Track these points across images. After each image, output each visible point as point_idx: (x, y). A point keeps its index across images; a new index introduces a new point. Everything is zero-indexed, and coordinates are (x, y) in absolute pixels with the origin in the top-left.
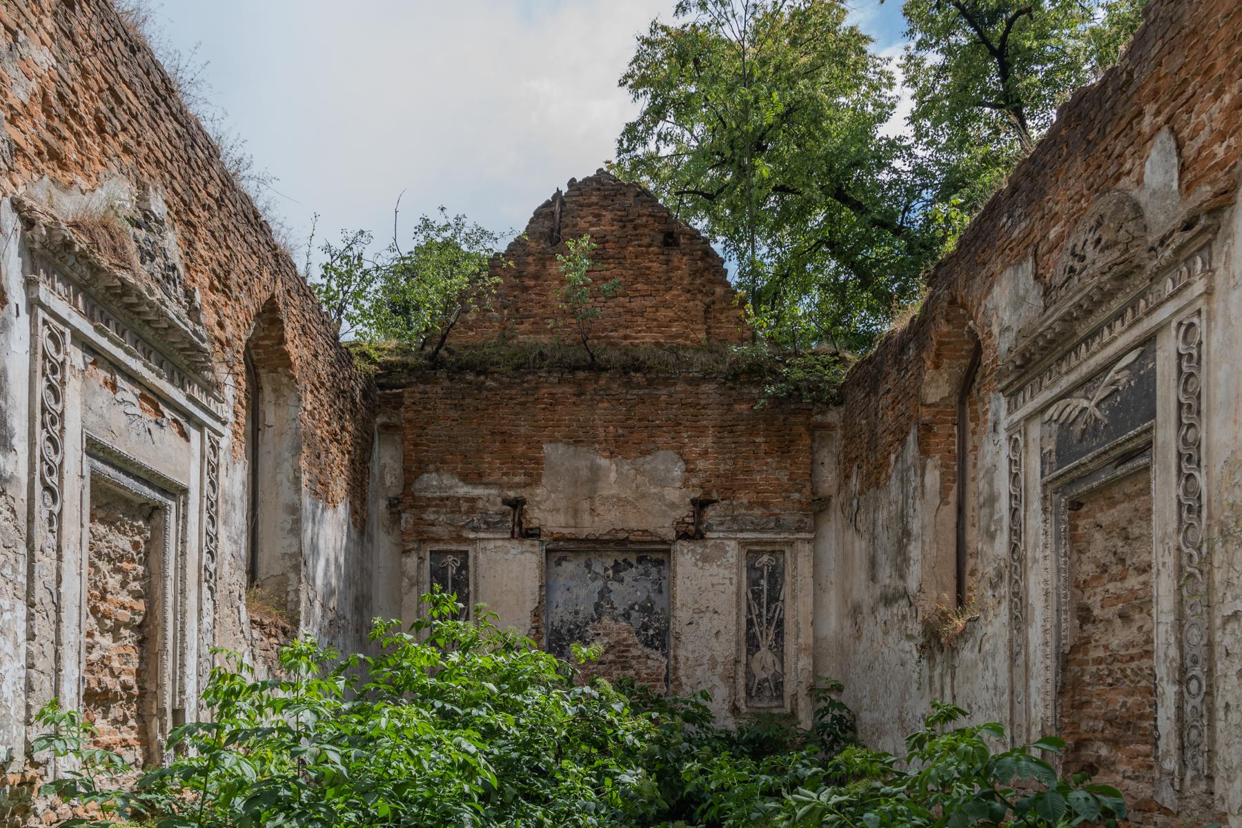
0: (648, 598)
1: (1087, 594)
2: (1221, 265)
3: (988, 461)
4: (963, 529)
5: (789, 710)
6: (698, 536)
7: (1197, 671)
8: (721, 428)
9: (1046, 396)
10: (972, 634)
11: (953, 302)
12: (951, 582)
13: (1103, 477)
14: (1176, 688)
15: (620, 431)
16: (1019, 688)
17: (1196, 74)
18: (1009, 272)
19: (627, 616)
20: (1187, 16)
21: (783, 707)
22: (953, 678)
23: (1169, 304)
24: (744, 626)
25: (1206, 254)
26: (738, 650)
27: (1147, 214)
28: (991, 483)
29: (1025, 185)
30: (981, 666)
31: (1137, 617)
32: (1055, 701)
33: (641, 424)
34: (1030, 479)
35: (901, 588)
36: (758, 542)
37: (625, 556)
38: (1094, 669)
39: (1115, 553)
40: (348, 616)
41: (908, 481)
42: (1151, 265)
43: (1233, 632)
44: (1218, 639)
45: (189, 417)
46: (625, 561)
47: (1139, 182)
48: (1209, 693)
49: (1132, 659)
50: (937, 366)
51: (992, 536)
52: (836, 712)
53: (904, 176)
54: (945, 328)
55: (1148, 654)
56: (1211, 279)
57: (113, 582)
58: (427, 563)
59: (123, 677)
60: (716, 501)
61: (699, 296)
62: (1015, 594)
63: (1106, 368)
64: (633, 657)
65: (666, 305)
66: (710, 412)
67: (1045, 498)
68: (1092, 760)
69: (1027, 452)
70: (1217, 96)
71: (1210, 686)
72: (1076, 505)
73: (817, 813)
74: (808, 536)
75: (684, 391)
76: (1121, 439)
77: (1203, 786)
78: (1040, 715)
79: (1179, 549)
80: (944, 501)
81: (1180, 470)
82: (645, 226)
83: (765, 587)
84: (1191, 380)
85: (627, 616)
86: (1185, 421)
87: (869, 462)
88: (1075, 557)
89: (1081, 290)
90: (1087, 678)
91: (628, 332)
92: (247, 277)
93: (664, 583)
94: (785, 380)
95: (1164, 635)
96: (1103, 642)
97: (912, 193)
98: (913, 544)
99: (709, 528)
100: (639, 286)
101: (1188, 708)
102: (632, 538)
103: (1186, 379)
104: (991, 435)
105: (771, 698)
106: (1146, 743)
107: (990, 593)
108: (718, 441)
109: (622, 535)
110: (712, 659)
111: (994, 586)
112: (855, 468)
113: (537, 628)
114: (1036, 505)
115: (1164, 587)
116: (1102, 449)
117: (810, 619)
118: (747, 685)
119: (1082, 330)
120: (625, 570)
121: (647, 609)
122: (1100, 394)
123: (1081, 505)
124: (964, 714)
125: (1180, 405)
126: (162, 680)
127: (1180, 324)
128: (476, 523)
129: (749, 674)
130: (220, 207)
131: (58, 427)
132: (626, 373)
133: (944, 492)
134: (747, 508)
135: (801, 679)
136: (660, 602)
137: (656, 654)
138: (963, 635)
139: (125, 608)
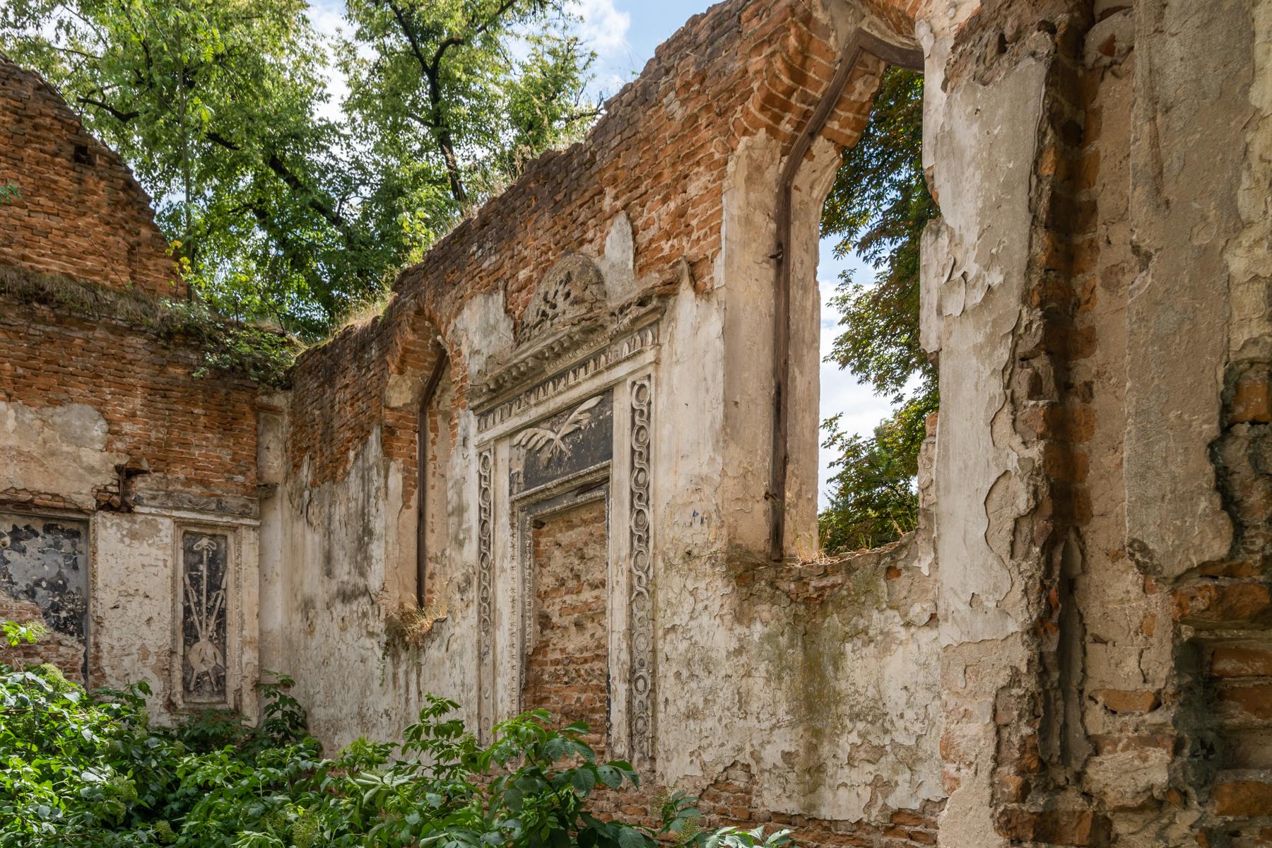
0: (60, 574)
1: (546, 604)
3: (457, 472)
4: (424, 533)
5: (232, 706)
6: (124, 509)
7: (643, 672)
8: (152, 390)
10: (439, 634)
11: (419, 312)
12: (411, 583)
13: (565, 503)
14: (626, 686)
15: (20, 371)
16: (486, 685)
17: (647, 176)
18: (479, 299)
19: (30, 593)
20: (641, 124)
21: (225, 702)
22: (419, 675)
23: (625, 364)
24: (181, 615)
25: (655, 330)
27: (607, 283)
28: (460, 494)
29: (495, 221)
30: (448, 664)
31: (589, 625)
33: (50, 367)
34: (499, 495)
35: (361, 585)
36: (197, 524)
37: (27, 522)
38: (552, 669)
39: (572, 570)
41: (370, 480)
42: (612, 328)
43: (672, 642)
44: (660, 647)
46: (27, 527)
47: (601, 252)
48: (653, 690)
49: (586, 661)
50: (401, 372)
51: (461, 544)
52: (288, 708)
53: (341, 165)
54: (411, 337)
55: (604, 658)
56: (659, 351)
60: (146, 472)
61: (121, 232)
62: (484, 599)
63: (571, 407)
65: (77, 231)
66: (138, 370)
67: (513, 514)
70: (665, 200)
71: (654, 684)
72: (539, 524)
73: (382, 796)
74: (253, 523)
75: (106, 340)
76: (582, 472)
77: (647, 766)
78: (506, 709)
79: (630, 571)
80: (406, 505)
81: (632, 505)
82: (49, 130)
83: (205, 574)
84: (642, 432)
85: (30, 593)
87: (324, 455)
88: (537, 570)
89: (554, 334)
90: (546, 677)
91: (27, 252)
93: (81, 559)
94: (227, 351)
97: (349, 185)
98: (376, 543)
99: (138, 501)
100: (42, 200)
101: (636, 703)
102: (37, 501)
103: (638, 430)
104: (461, 448)
105: (212, 694)
106: (596, 732)
107: (458, 596)
108: (149, 404)
109: (24, 497)
110: (143, 648)
111: (462, 591)
112: (306, 458)
114: (504, 519)
115: (617, 602)
116: (566, 478)
117: (256, 610)
118: (184, 679)
119: (551, 370)
120: (28, 538)
121: (58, 587)
122: (566, 429)
123: (543, 524)
124: (456, 706)
125: (633, 451)
127: (634, 383)
129: (187, 666)
132: (27, 302)
133: (406, 495)
134: (183, 484)
136: (75, 581)
137: (71, 641)
138: (429, 635)
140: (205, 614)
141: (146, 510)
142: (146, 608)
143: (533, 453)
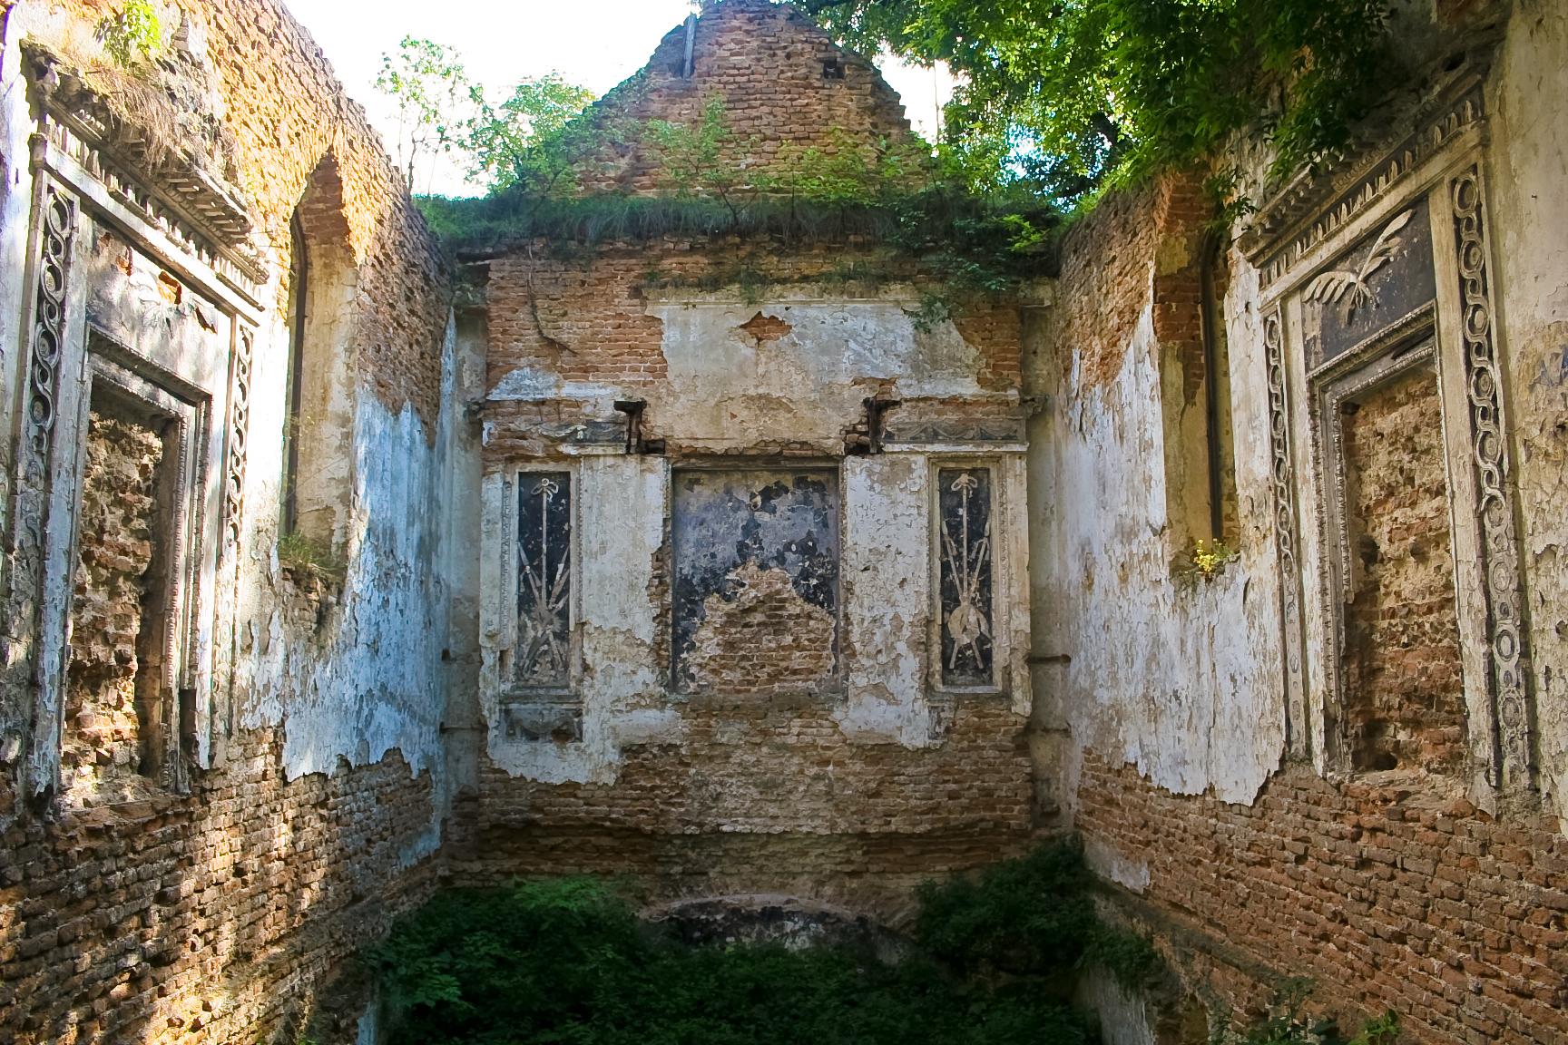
0: (809, 533)
2: (1495, 111)
5: (1000, 688)
9: (1304, 268)
13: (1380, 370)
14: (1484, 648)
19: (780, 559)
23: (1438, 157)
26: (931, 606)
28: (1245, 379)
31: (1432, 553)
32: (1339, 668)
36: (955, 458)
37: (779, 477)
38: (1385, 624)
39: (1402, 471)
40: (411, 562)
44: (1531, 583)
45: (217, 301)
48: (1525, 654)
49: (1430, 610)
55: (1447, 603)
57: (113, 518)
58: (516, 489)
59: (119, 647)
64: (790, 617)
68: (1389, 747)
69: (1287, 339)
79: (1475, 465)
86: (1470, 302)
88: (1353, 475)
90: (1377, 637)
92: (301, 125)
93: (831, 513)
95: (1466, 578)
96: (1394, 588)
100: (795, 127)
101: (1501, 676)
102: (786, 452)
103: (1465, 249)
106: (1454, 723)
109: (773, 449)
113: (659, 577)
114: (1302, 407)
116: (1375, 336)
118: (943, 653)
121: (807, 550)
122: (1369, 266)
123: (1356, 408)
126: (168, 650)
127: (1454, 182)
128: (580, 435)
130: (272, 45)
131: (57, 318)
135: (1015, 644)
137: (819, 612)
139: (126, 554)
140: (966, 571)
141: (897, 448)
142: (900, 568)
143: (1330, 304)
